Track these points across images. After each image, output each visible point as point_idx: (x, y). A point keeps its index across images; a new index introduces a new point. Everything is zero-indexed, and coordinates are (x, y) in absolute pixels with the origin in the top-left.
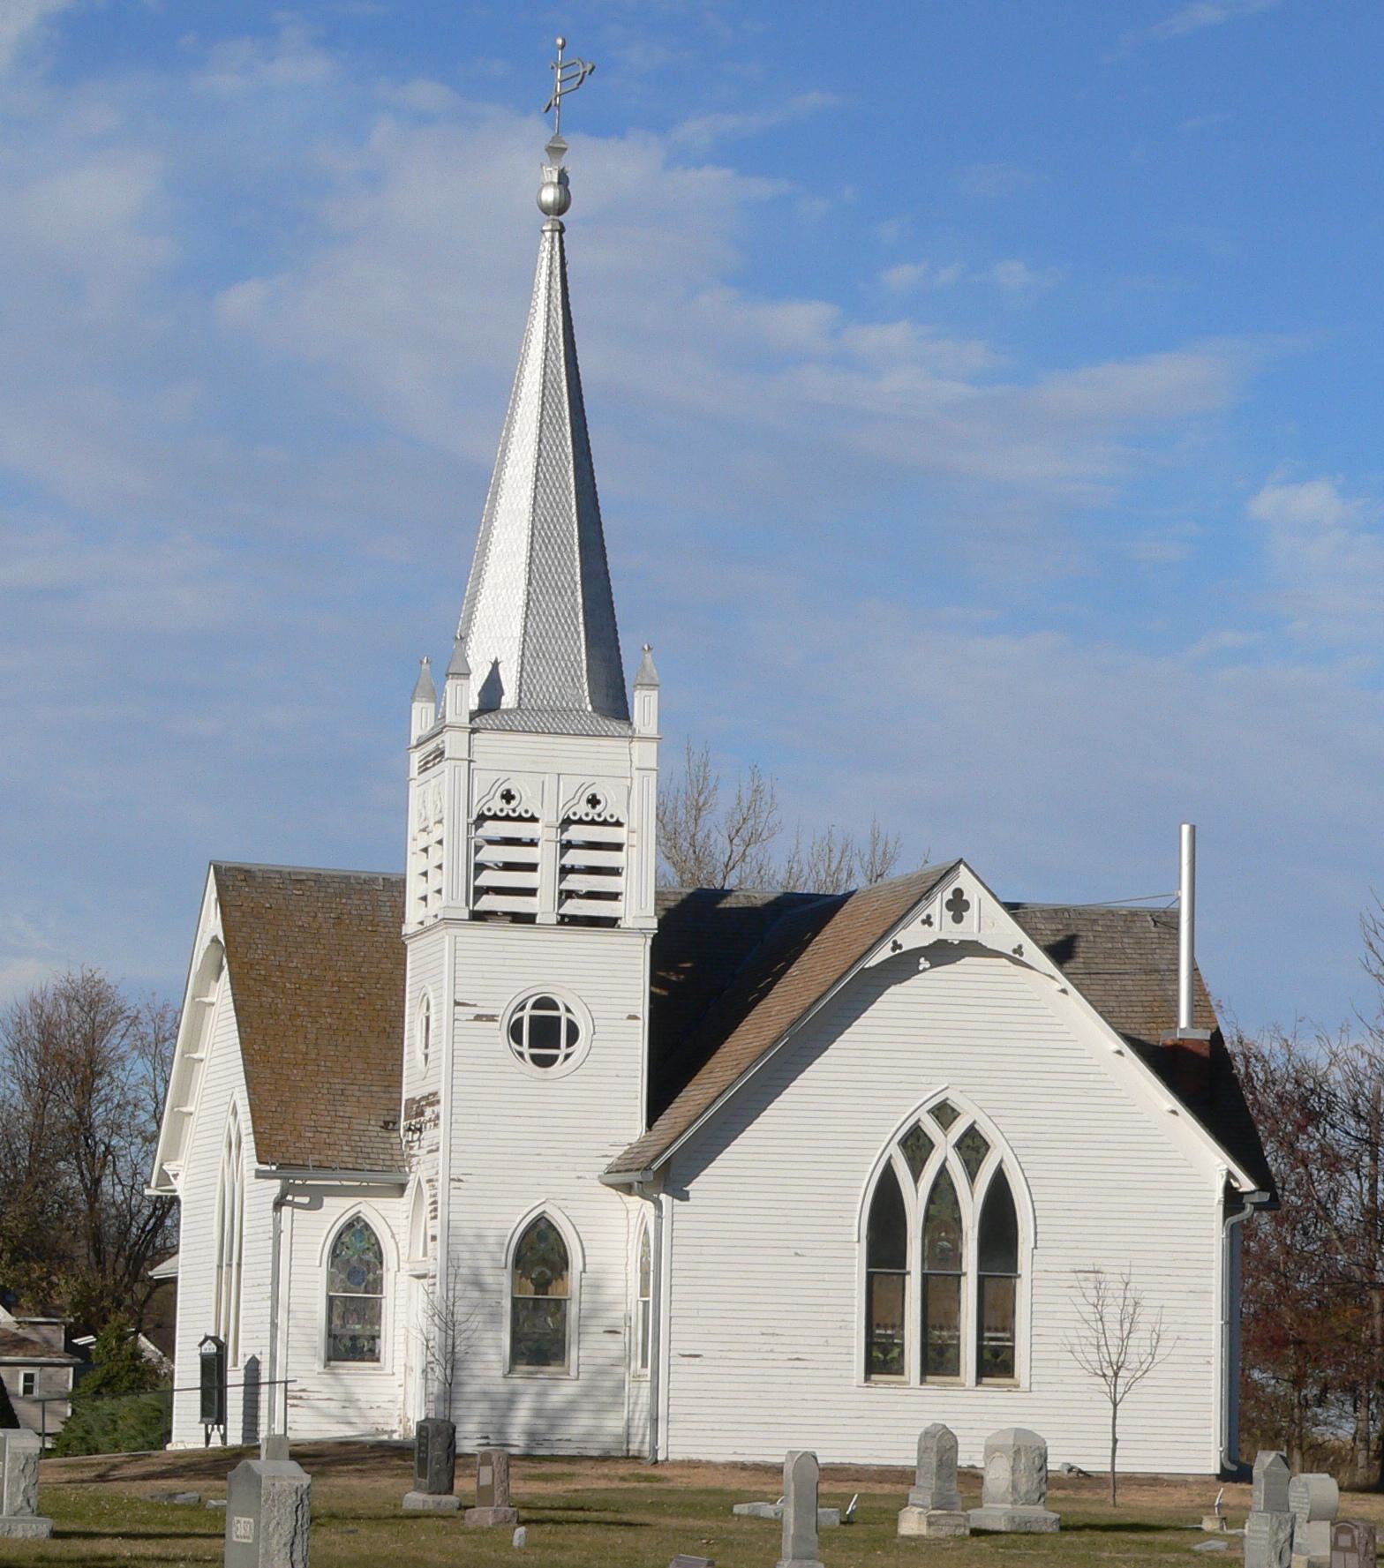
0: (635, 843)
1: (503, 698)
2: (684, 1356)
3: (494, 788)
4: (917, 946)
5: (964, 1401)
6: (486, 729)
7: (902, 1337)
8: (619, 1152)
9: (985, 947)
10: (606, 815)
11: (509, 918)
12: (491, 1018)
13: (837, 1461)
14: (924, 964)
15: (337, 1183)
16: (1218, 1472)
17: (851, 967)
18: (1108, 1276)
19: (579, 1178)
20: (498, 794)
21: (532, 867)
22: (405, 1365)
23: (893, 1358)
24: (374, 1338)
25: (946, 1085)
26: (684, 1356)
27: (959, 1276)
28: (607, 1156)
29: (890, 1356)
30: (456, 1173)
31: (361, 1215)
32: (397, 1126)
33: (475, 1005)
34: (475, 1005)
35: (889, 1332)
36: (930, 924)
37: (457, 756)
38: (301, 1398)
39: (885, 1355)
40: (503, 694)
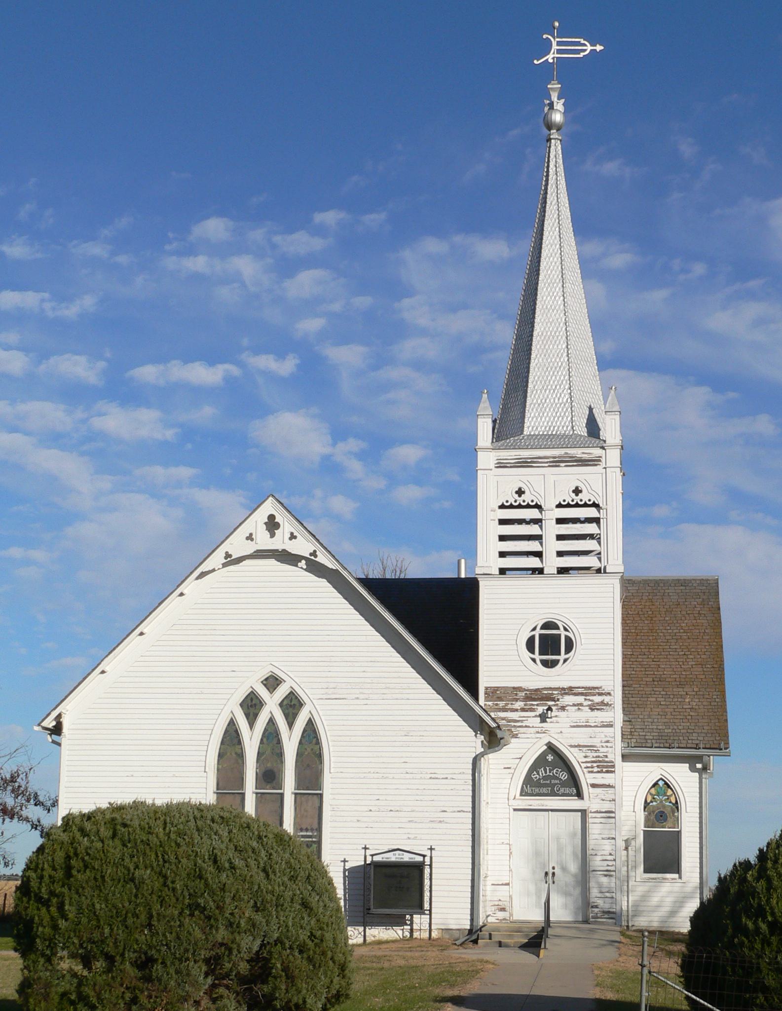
1: (601, 432)
3: (530, 486)
4: (240, 556)
9: (290, 553)
11: (531, 572)
14: (537, 572)
21: (560, 537)
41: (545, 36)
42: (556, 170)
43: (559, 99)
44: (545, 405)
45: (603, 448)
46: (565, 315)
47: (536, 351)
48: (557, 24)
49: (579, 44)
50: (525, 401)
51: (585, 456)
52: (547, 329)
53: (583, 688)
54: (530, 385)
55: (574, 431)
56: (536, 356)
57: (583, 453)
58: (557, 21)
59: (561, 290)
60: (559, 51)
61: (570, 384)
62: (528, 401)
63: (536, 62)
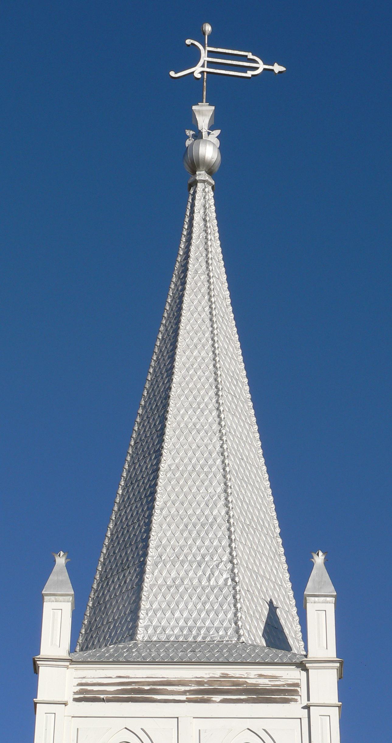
41: (188, 42)
42: (205, 225)
43: (212, 128)
44: (181, 589)
45: (302, 666)
46: (221, 439)
47: (165, 497)
48: (208, 28)
49: (244, 58)
50: (141, 581)
51: (264, 683)
52: (186, 460)
54: (152, 552)
55: (239, 637)
56: (165, 503)
57: (261, 676)
58: (206, 22)
59: (214, 400)
60: (211, 64)
61: (231, 554)
62: (146, 580)
63: (172, 74)
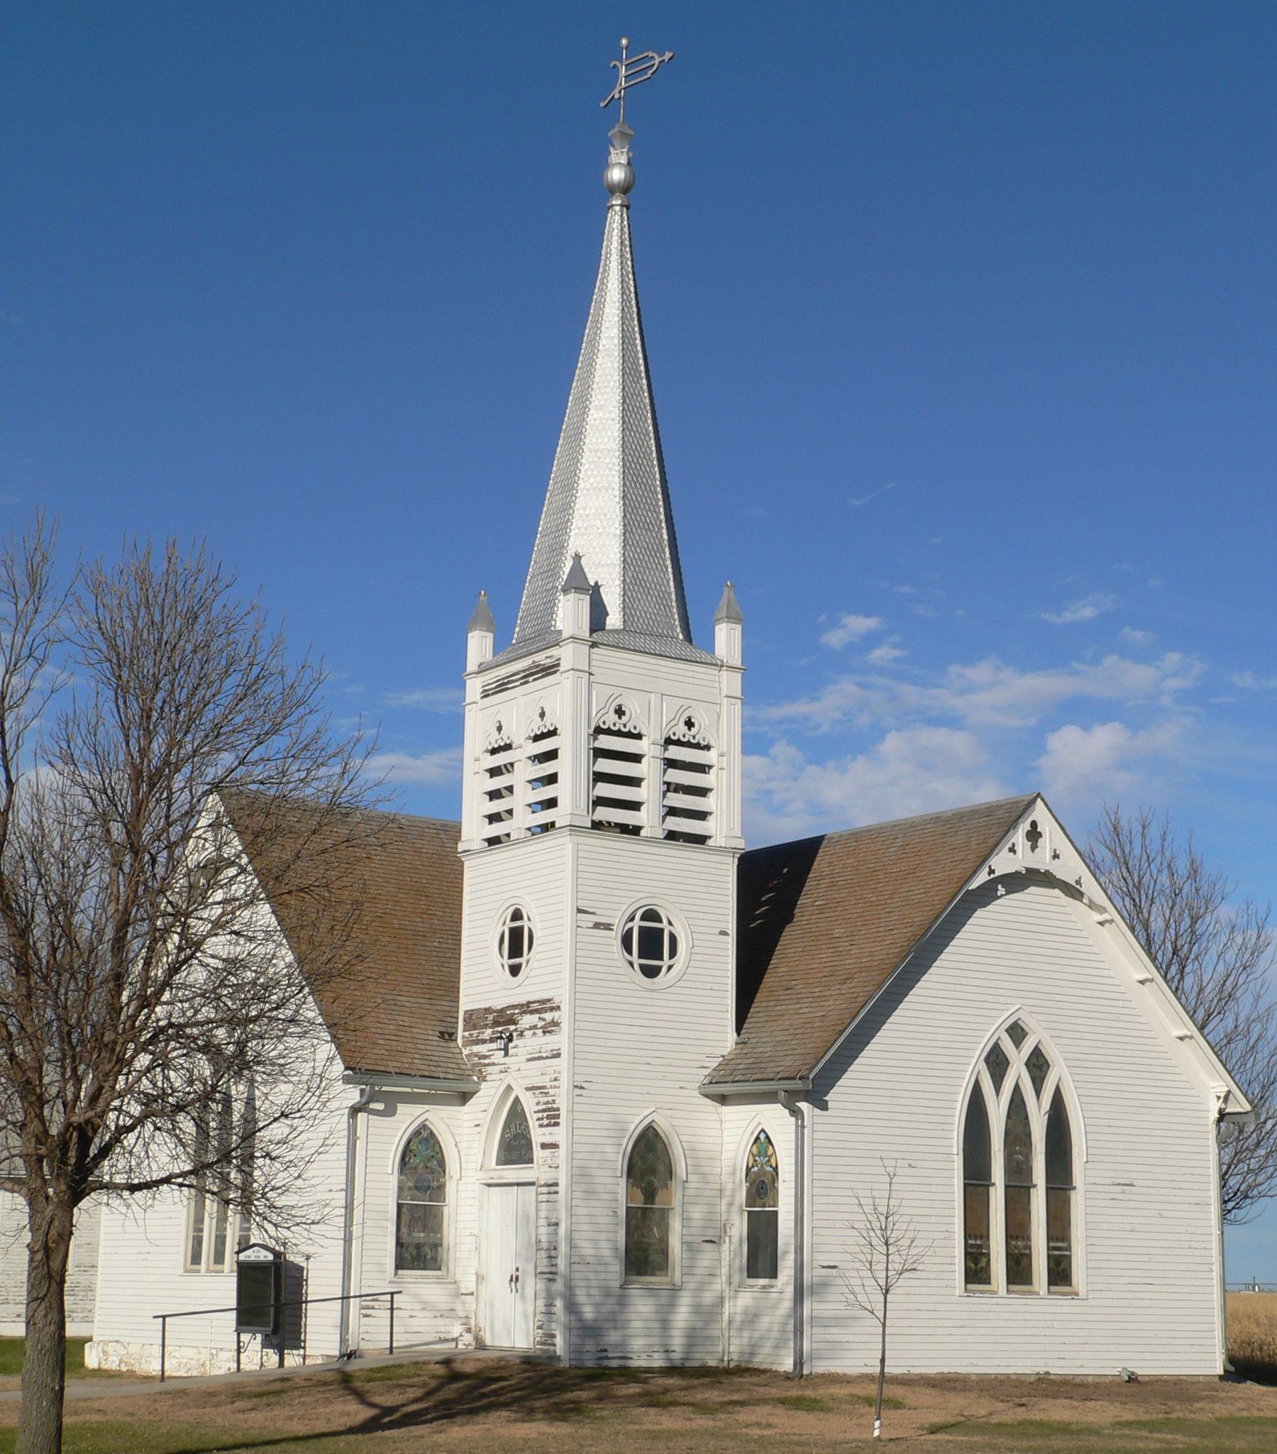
0: (725, 766)
1: (608, 618)
2: (823, 1267)
5: (1038, 1309)
6: (604, 645)
7: (988, 1248)
8: (714, 1063)
10: (698, 739)
11: (618, 830)
12: (608, 927)
13: (946, 1370)
15: (409, 1090)
16: (1222, 1373)
17: (959, 890)
18: (1242, 1189)
19: (681, 1088)
20: (612, 709)
22: (477, 1274)
23: (982, 1268)
24: (437, 1246)
25: (1018, 1006)
26: (823, 1267)
27: (1028, 1188)
28: (704, 1067)
29: (979, 1266)
30: (579, 1079)
31: (427, 1123)
32: (453, 1038)
33: (594, 913)
34: (594, 913)
35: (978, 1242)
36: (1015, 852)
37: (580, 668)
38: (373, 1308)
39: (976, 1265)
40: (607, 614)
53: (538, 1002)
57: (547, 657)
